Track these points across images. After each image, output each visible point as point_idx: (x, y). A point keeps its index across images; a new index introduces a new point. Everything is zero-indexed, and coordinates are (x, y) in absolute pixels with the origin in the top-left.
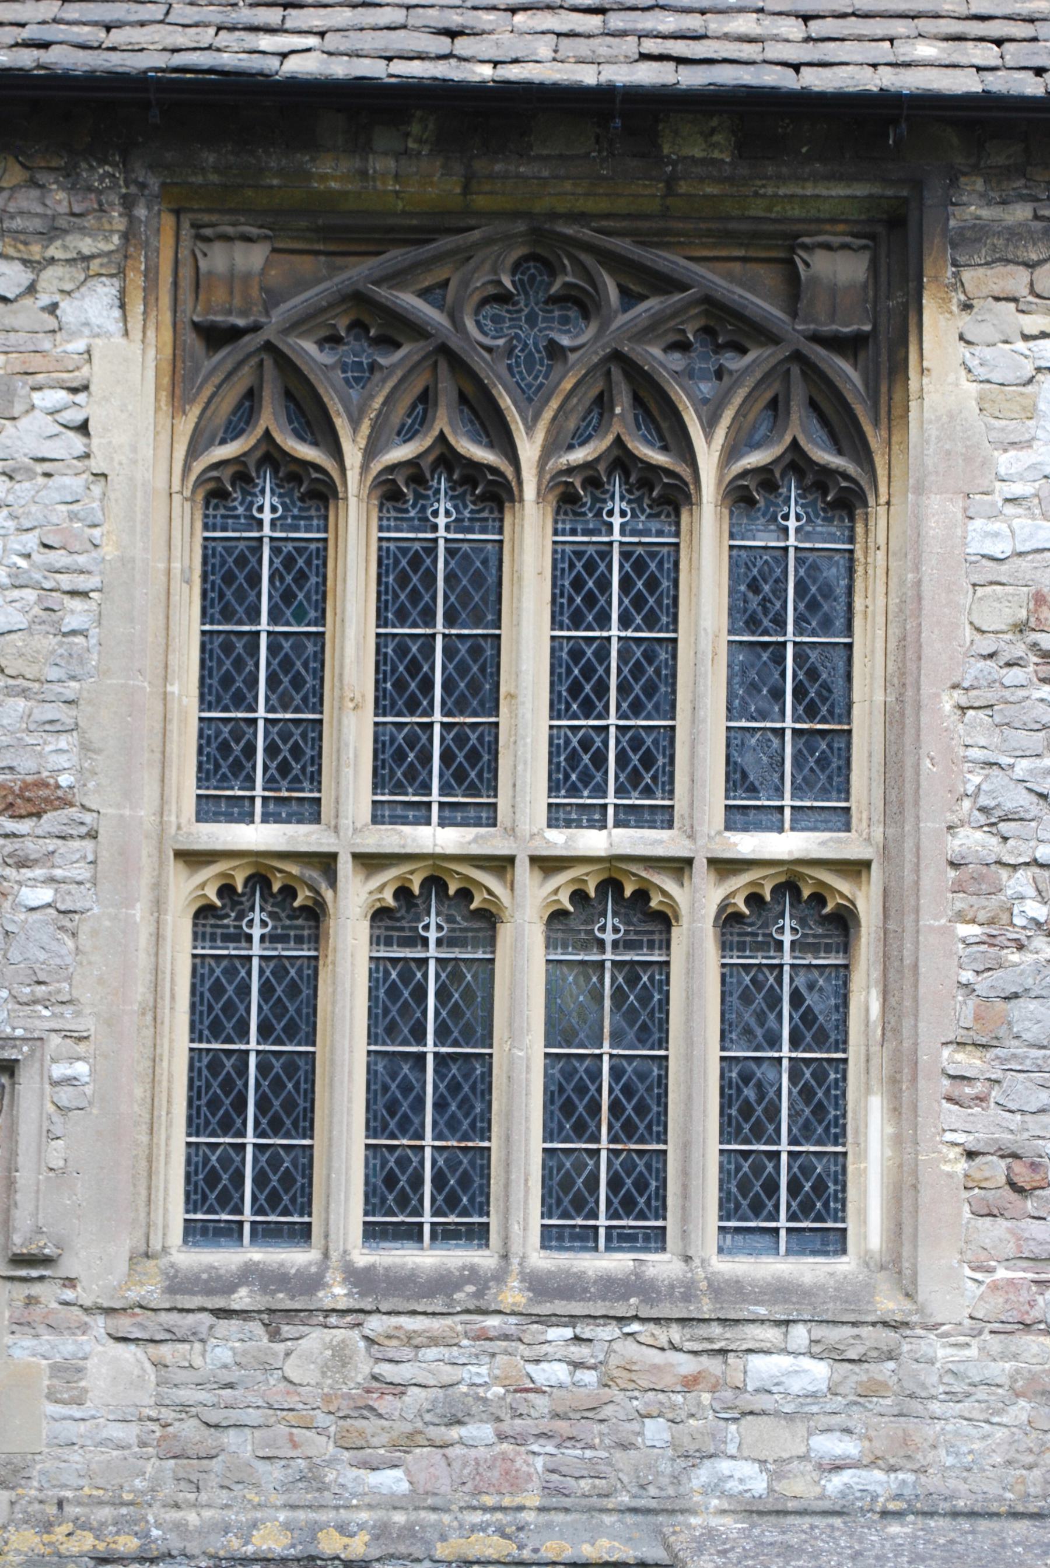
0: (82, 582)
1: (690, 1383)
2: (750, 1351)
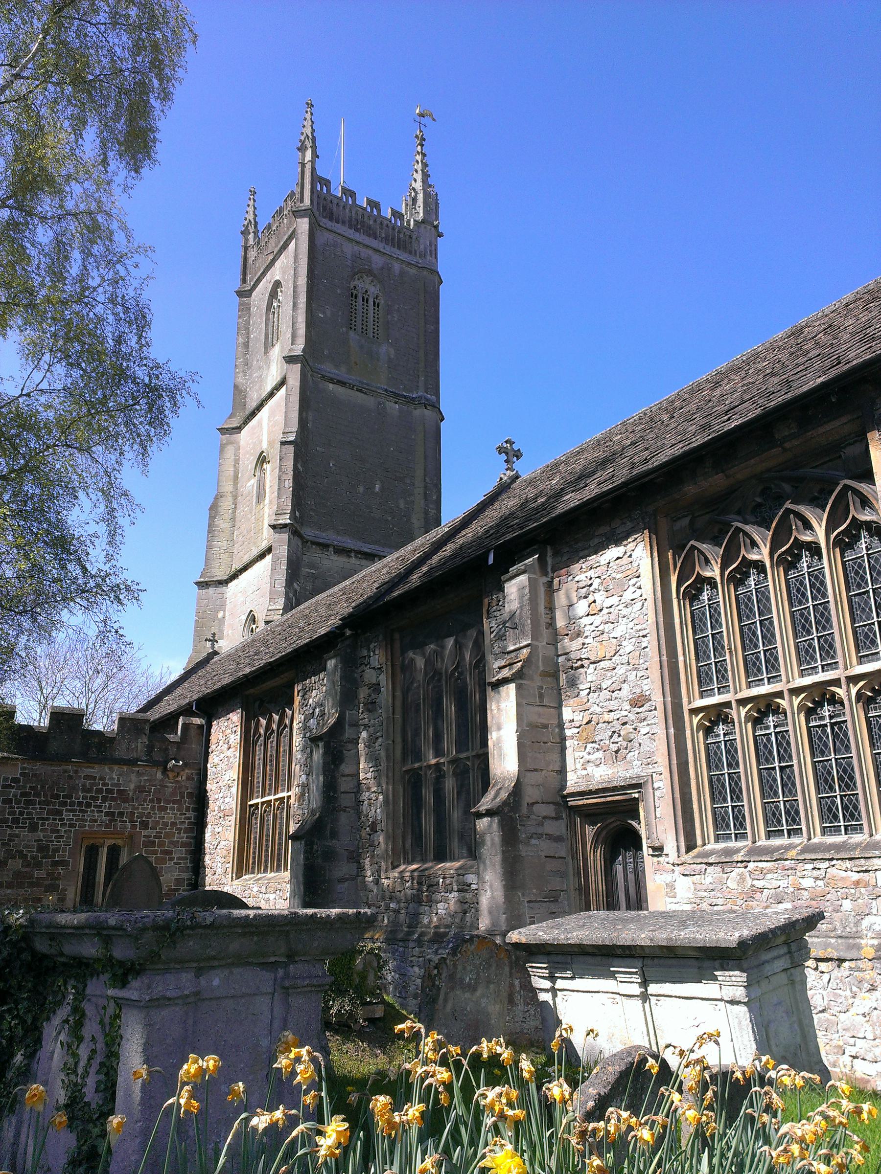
0: (644, 632)
1: (857, 883)
2: (876, 870)
